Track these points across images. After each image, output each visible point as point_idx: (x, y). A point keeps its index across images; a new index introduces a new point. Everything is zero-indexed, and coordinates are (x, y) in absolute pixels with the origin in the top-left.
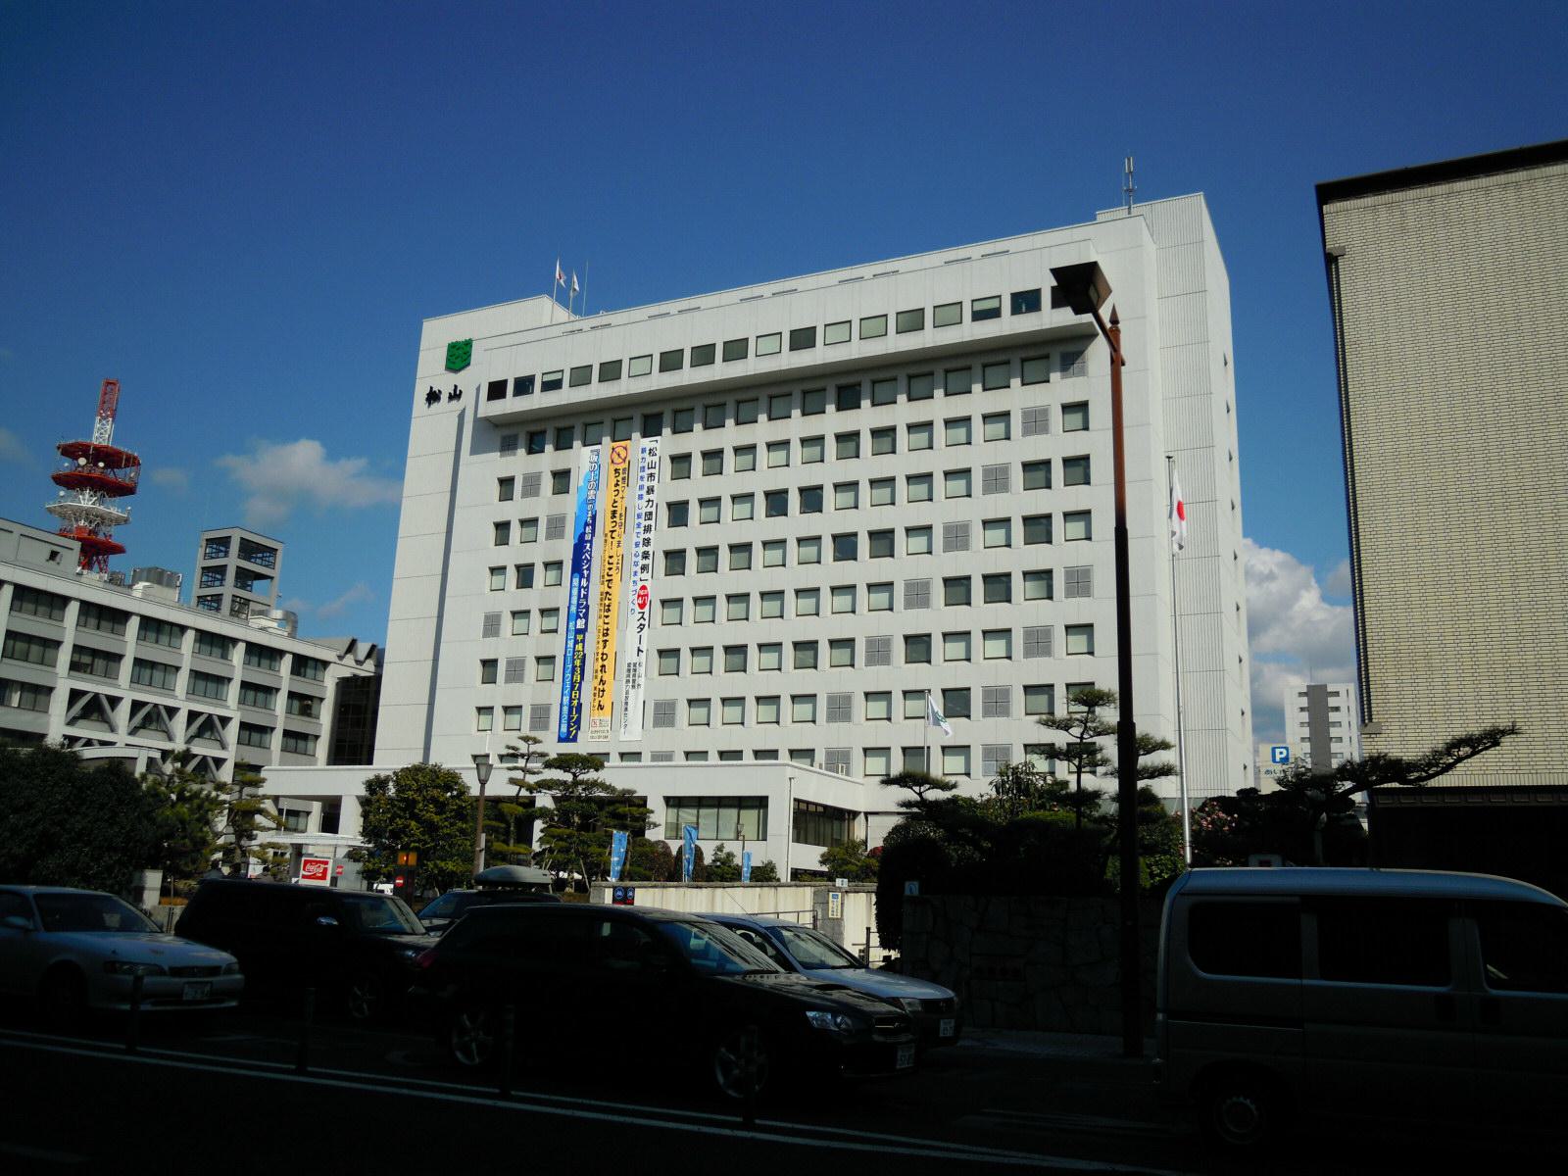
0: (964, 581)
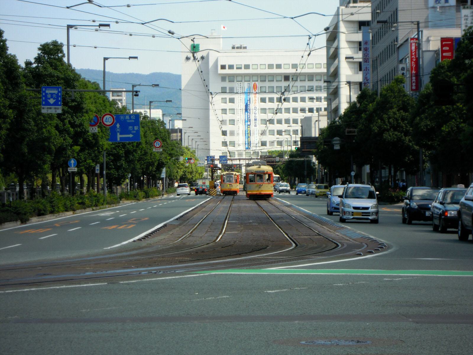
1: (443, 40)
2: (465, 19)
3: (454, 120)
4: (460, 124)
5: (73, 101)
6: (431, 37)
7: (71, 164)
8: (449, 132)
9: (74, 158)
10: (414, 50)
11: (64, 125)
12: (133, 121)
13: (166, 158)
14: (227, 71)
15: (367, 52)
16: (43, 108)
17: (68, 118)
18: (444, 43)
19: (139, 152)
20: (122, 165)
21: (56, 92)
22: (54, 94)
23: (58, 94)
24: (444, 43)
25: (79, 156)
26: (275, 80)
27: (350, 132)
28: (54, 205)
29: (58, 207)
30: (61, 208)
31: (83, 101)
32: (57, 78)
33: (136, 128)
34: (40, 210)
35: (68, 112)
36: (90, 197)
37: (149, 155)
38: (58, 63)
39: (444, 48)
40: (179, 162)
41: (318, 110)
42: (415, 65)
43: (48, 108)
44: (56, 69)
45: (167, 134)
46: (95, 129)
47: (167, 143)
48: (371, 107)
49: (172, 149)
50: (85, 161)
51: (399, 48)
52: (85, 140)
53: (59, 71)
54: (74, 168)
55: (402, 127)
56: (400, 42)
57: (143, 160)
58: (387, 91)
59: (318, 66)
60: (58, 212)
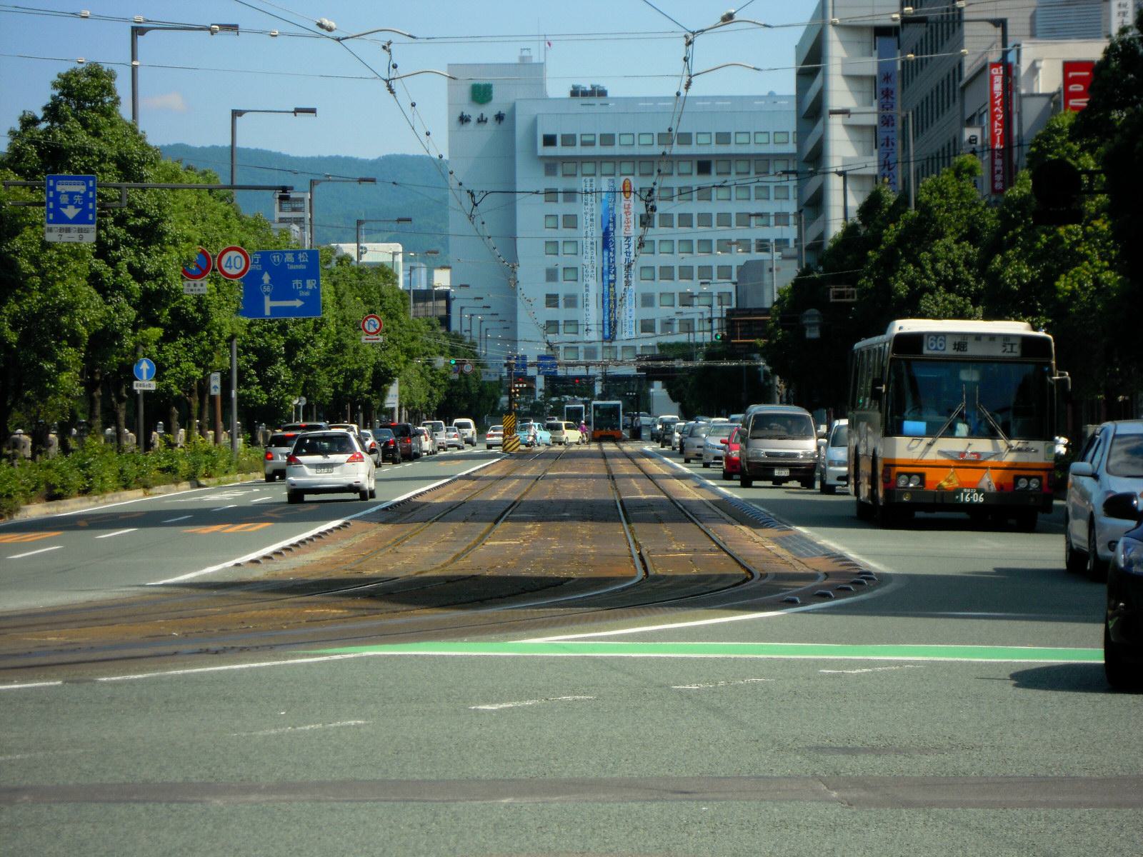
0: (709, 242)
1: (1068, 66)
2: (1119, 14)
3: (1086, 263)
4: (1101, 272)
5: (139, 213)
6: (1041, 60)
7: (140, 372)
8: (1073, 292)
9: (150, 357)
10: (999, 94)
11: (117, 274)
12: (304, 267)
13: (396, 358)
14: (558, 150)
15: (890, 100)
16: (50, 230)
17: (127, 256)
18: (1071, 74)
19: (321, 344)
20: (278, 375)
21: (81, 189)
22: (78, 193)
23: (85, 195)
24: (1071, 74)
25: (164, 352)
26: (675, 172)
27: (840, 295)
28: (90, 473)
29: (102, 479)
30: (110, 481)
31: (163, 215)
32: (98, 156)
33: (310, 284)
34: (51, 487)
35: (128, 243)
36: (193, 454)
37: (351, 350)
38: (103, 121)
39: (1072, 88)
40: (436, 370)
41: (781, 243)
42: (1001, 130)
43: (61, 230)
44: (96, 134)
45: (399, 302)
46: (202, 285)
47: (400, 321)
48: (891, 233)
49: (413, 339)
50: (177, 364)
51: (963, 89)
52: (175, 313)
53: (104, 140)
54: (147, 383)
55: (967, 283)
56: (967, 73)
57: (337, 366)
58: (931, 194)
59: (780, 138)
60: (103, 491)
